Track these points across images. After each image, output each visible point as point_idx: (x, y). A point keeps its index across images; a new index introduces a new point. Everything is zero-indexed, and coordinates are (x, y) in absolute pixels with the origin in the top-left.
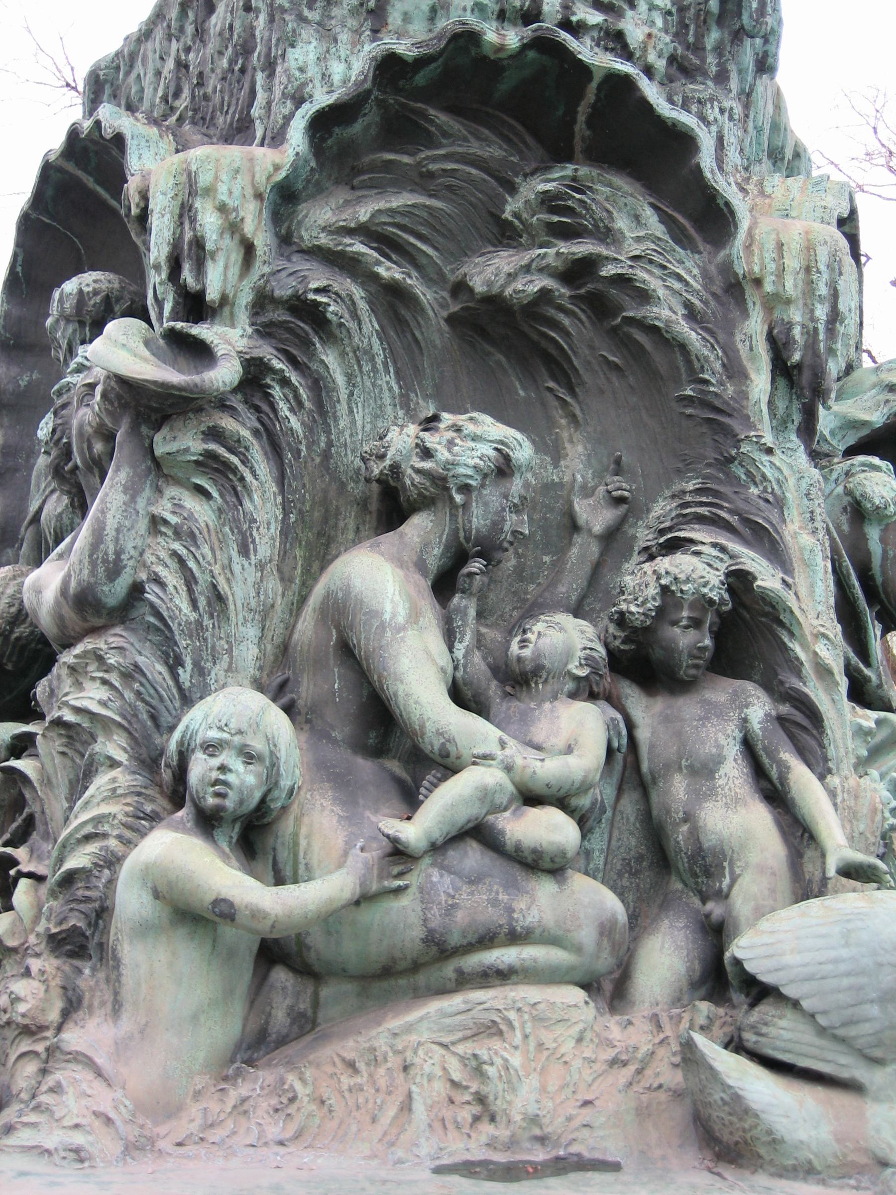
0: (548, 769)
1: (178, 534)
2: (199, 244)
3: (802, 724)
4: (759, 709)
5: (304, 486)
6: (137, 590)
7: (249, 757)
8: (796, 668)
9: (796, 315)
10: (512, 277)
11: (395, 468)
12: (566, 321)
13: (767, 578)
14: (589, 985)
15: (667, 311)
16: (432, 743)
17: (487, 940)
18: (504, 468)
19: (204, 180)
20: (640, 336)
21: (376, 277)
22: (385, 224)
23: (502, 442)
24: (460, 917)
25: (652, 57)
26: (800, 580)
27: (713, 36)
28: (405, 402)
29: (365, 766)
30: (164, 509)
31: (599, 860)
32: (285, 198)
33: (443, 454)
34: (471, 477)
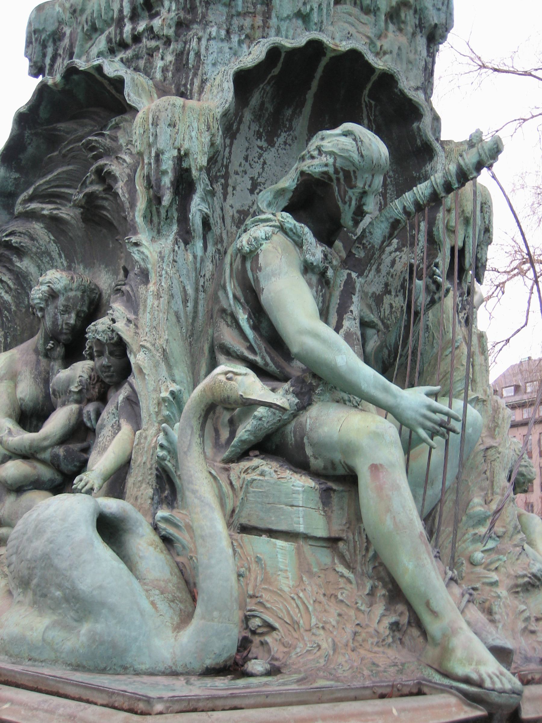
5: (16, 324)
21: (44, 216)
22: (46, 189)
23: (49, 282)
34: (39, 303)
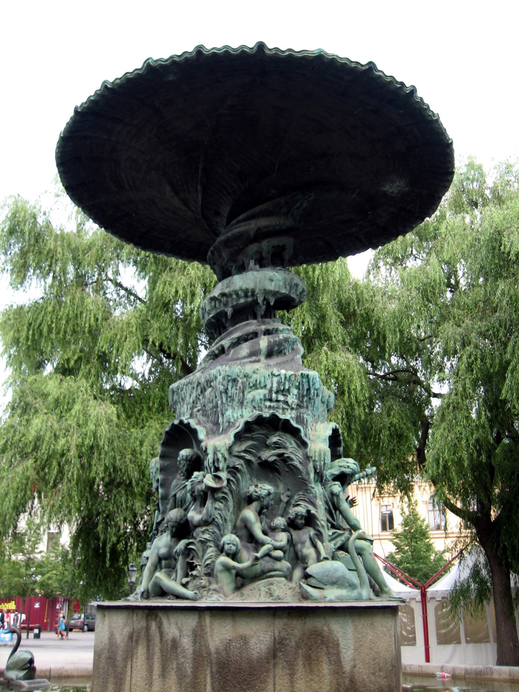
0: (278, 544)
1: (219, 510)
2: (218, 460)
3: (319, 535)
7: (234, 545)
8: (318, 526)
9: (318, 464)
11: (251, 495)
13: (313, 511)
14: (286, 577)
15: (296, 463)
16: (260, 541)
17: (270, 571)
18: (269, 494)
19: (219, 449)
25: (293, 406)
26: (319, 511)
27: (305, 399)
28: (251, 479)
29: (250, 545)
30: (217, 506)
31: (287, 558)
32: (230, 450)
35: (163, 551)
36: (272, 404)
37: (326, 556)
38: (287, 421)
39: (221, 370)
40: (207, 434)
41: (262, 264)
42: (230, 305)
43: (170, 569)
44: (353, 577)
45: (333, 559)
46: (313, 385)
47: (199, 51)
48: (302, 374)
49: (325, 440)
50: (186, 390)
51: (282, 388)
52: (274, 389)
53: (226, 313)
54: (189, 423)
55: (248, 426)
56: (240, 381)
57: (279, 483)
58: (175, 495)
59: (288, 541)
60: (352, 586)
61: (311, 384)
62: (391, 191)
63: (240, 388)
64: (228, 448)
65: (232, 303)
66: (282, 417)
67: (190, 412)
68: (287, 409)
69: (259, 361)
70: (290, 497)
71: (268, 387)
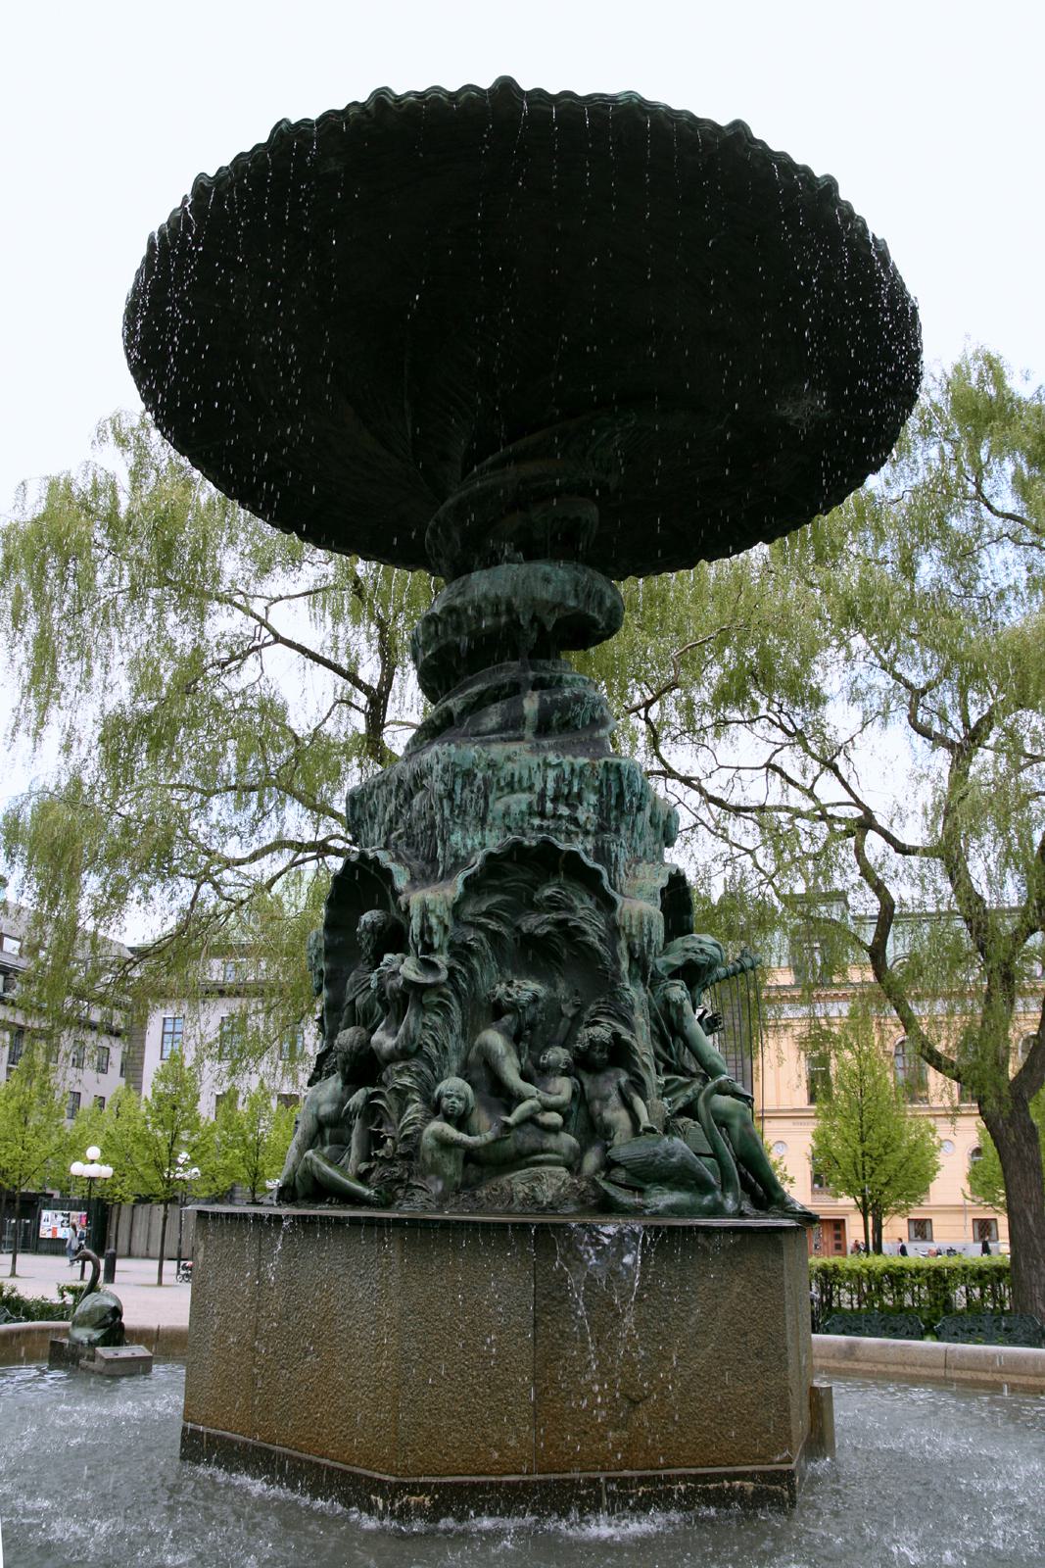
0: (552, 1099)
1: (431, 1028)
2: (430, 928)
3: (638, 1085)
4: (624, 1078)
6: (420, 1047)
7: (460, 1098)
8: (635, 1064)
10: (536, 927)
11: (499, 1000)
12: (557, 941)
13: (626, 1036)
15: (593, 939)
17: (535, 1152)
18: (535, 999)
19: (431, 907)
20: (583, 947)
24: (526, 1145)
25: (589, 827)
26: (638, 1034)
27: (613, 814)
28: (500, 971)
32: (456, 909)
33: (515, 997)
35: (327, 1109)
36: (545, 823)
37: (649, 1125)
38: (574, 855)
39: (440, 753)
40: (413, 880)
41: (531, 552)
42: (466, 631)
43: (341, 1146)
44: (706, 1167)
45: (666, 1131)
46: (630, 786)
47: (381, 97)
48: (606, 763)
49: (653, 895)
50: (377, 797)
51: (566, 791)
52: (550, 792)
53: (458, 646)
54: (377, 858)
55: (494, 863)
56: (480, 775)
57: (558, 978)
58: (353, 1001)
59: (574, 1093)
60: (702, 1186)
61: (625, 783)
62: (795, 418)
63: (479, 789)
64: (450, 905)
65: (469, 626)
66: (563, 846)
67: (383, 840)
68: (577, 834)
69: (520, 739)
70: (581, 1008)
71: (538, 788)
